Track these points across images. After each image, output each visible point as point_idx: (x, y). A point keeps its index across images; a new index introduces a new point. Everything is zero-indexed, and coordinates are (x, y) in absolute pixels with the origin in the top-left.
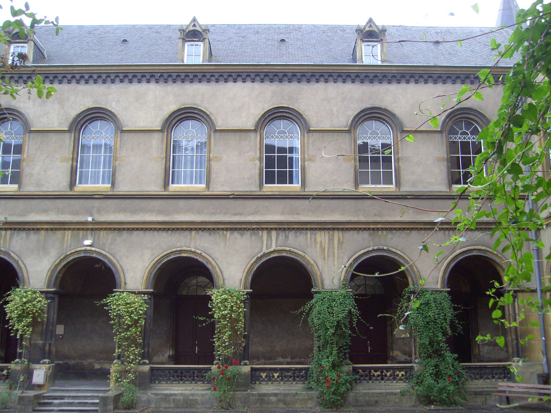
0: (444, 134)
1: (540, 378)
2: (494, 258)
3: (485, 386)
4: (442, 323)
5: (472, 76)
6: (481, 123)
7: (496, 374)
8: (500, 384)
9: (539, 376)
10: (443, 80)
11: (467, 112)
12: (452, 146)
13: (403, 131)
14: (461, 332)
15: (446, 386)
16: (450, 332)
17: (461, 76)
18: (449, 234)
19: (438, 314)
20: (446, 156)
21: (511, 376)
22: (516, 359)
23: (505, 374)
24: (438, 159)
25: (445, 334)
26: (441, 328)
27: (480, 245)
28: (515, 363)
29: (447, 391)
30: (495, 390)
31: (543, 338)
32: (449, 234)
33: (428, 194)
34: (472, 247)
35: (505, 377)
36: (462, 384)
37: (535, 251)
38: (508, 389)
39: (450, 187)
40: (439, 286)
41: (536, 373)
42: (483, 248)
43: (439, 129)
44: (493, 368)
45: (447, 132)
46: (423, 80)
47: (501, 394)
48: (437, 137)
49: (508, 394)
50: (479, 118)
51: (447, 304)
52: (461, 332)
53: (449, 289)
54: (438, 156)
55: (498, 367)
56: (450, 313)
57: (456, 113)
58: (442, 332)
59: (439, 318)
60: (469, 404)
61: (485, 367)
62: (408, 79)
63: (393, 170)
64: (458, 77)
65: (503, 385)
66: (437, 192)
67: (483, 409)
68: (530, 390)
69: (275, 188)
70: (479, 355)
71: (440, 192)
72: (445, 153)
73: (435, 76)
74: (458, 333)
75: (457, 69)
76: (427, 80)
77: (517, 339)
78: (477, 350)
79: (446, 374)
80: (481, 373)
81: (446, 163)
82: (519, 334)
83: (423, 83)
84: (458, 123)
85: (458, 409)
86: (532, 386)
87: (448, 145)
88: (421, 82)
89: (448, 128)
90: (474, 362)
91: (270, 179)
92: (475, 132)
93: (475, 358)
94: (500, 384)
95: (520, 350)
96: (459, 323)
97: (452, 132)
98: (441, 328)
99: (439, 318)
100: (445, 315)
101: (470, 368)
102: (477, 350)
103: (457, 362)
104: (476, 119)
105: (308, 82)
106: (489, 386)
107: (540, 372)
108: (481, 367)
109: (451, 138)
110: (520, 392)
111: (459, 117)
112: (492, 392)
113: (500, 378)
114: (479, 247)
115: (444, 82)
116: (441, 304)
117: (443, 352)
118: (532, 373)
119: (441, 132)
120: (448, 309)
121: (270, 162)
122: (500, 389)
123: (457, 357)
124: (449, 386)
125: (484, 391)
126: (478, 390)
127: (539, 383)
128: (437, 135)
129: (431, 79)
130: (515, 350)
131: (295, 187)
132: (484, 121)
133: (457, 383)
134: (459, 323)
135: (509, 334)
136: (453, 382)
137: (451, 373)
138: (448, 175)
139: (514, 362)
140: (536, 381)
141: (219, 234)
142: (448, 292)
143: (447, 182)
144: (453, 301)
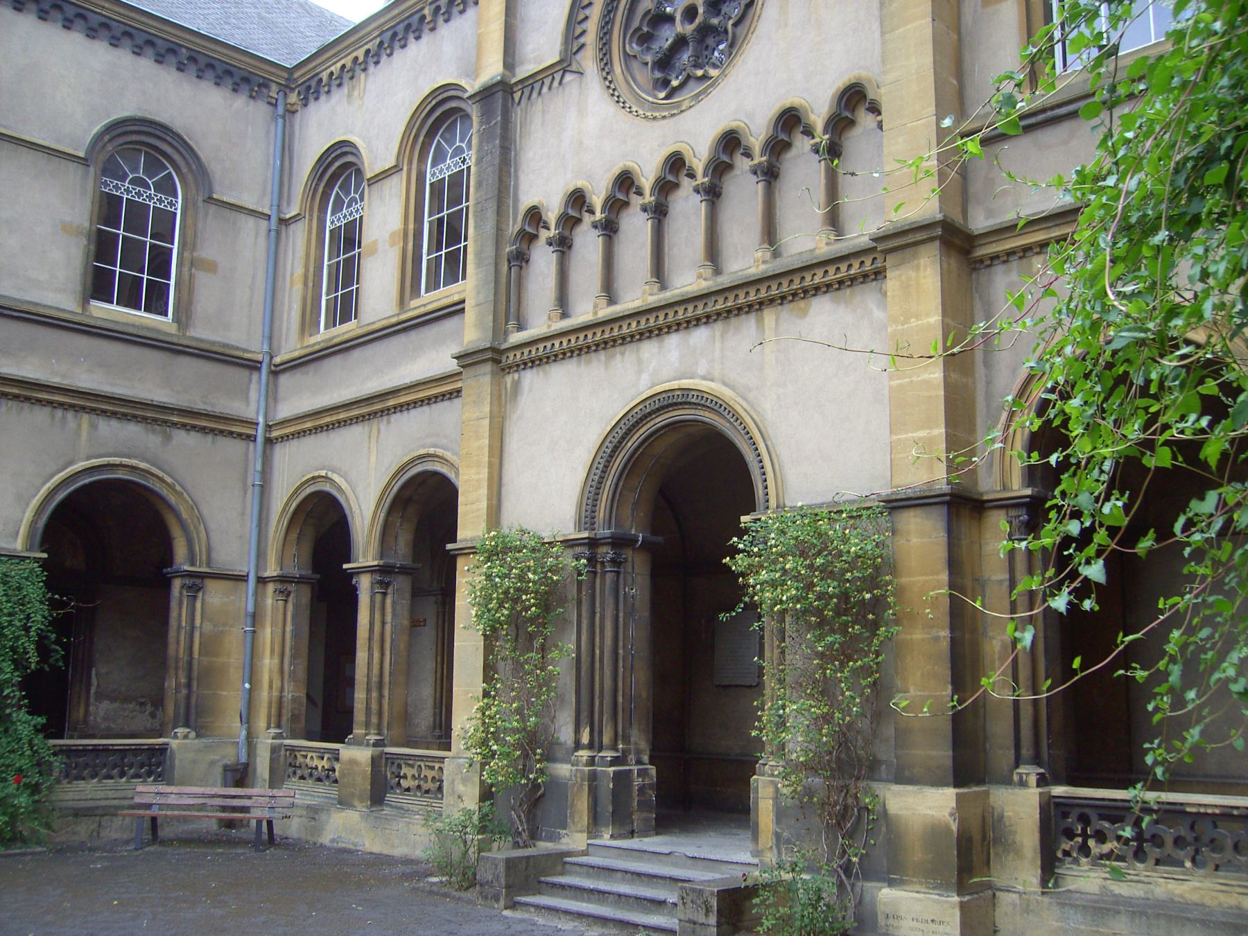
0: (92, 169)
1: (229, 774)
2: (164, 492)
3: (101, 795)
4: (17, 638)
5: (184, 50)
6: (185, 170)
7: (131, 766)
8: (140, 788)
9: (226, 769)
10: (113, 37)
11: (158, 133)
12: (109, 208)
13: (210, 200)
14: (61, 664)
15: (7, 796)
16: (34, 659)
17: (159, 42)
18: (64, 418)
19: (10, 615)
20: (87, 225)
21: (163, 770)
22: (181, 731)
23: (150, 765)
24: (66, 228)
25: (19, 664)
26: (13, 649)
27: (135, 457)
28: (177, 741)
29: (10, 810)
30: (126, 803)
31: (247, 686)
32: (64, 418)
33: (24, 307)
34: (117, 460)
35: (149, 774)
36: (50, 788)
37: (257, 489)
38: (158, 800)
39: (85, 302)
40: (18, 545)
41: (221, 763)
42: (143, 465)
43: (82, 154)
44: (123, 752)
45: (100, 165)
46: (60, 16)
47: (141, 812)
48: (73, 173)
49: (155, 811)
50: (181, 153)
51: (35, 591)
52: (61, 664)
53: (45, 555)
54: (68, 219)
55: (137, 750)
56: (39, 615)
57: (131, 128)
58: (14, 661)
59: (10, 623)
60: (58, 840)
61: (106, 750)
62: (47, 7)
63: (172, 282)
64: (150, 43)
65: (146, 791)
66: (51, 307)
67: (91, 849)
68: (210, 802)
69: (109, 311)
70: (86, 722)
71: (58, 309)
72: (87, 216)
73: (95, 20)
74: (50, 666)
75: (151, 22)
76: (71, 21)
77: (189, 685)
78: (82, 711)
79: (8, 766)
80: (87, 763)
81: (84, 241)
82: (195, 674)
83: (60, 24)
84: (130, 151)
85: (33, 854)
86: (209, 790)
87: (97, 199)
88: (54, 21)
89: (103, 157)
90: (71, 737)
91: (99, 286)
92: (166, 187)
93: (75, 730)
94: (140, 788)
95: (193, 710)
96: (58, 642)
97: (111, 170)
98: (13, 649)
99: (10, 623)
100: (28, 617)
101: (69, 752)
102: (82, 711)
103: (41, 736)
104: (176, 157)
105: (179, 69)
106: (111, 794)
107: (230, 760)
108: (96, 750)
109: (107, 185)
110: (179, 807)
111: (134, 138)
112: (117, 808)
113: (137, 776)
114: (133, 462)
115: (115, 42)
116: (19, 589)
117: (8, 711)
118: (213, 763)
119: (84, 162)
120: (37, 604)
121: (103, 246)
122: (137, 800)
123: (43, 725)
124: (15, 796)
125: (98, 808)
126: (82, 804)
127: (225, 785)
128: (72, 166)
129: (82, 22)
130: (182, 710)
131: (163, 323)
132: (194, 167)
133: (35, 789)
134: (58, 642)
135: (172, 672)
136: (27, 786)
137: (24, 763)
138: (85, 274)
139: (176, 737)
140: (219, 781)
141: (53, 417)
142: (44, 564)
143: (79, 288)
144: (49, 585)
